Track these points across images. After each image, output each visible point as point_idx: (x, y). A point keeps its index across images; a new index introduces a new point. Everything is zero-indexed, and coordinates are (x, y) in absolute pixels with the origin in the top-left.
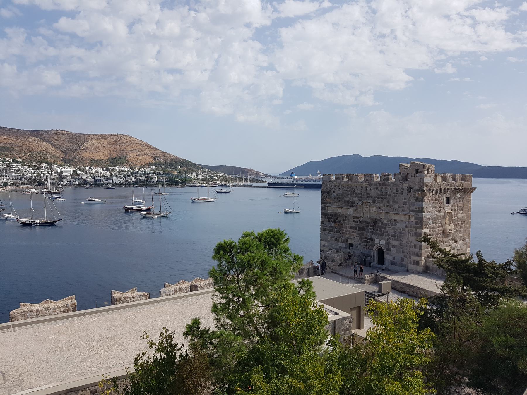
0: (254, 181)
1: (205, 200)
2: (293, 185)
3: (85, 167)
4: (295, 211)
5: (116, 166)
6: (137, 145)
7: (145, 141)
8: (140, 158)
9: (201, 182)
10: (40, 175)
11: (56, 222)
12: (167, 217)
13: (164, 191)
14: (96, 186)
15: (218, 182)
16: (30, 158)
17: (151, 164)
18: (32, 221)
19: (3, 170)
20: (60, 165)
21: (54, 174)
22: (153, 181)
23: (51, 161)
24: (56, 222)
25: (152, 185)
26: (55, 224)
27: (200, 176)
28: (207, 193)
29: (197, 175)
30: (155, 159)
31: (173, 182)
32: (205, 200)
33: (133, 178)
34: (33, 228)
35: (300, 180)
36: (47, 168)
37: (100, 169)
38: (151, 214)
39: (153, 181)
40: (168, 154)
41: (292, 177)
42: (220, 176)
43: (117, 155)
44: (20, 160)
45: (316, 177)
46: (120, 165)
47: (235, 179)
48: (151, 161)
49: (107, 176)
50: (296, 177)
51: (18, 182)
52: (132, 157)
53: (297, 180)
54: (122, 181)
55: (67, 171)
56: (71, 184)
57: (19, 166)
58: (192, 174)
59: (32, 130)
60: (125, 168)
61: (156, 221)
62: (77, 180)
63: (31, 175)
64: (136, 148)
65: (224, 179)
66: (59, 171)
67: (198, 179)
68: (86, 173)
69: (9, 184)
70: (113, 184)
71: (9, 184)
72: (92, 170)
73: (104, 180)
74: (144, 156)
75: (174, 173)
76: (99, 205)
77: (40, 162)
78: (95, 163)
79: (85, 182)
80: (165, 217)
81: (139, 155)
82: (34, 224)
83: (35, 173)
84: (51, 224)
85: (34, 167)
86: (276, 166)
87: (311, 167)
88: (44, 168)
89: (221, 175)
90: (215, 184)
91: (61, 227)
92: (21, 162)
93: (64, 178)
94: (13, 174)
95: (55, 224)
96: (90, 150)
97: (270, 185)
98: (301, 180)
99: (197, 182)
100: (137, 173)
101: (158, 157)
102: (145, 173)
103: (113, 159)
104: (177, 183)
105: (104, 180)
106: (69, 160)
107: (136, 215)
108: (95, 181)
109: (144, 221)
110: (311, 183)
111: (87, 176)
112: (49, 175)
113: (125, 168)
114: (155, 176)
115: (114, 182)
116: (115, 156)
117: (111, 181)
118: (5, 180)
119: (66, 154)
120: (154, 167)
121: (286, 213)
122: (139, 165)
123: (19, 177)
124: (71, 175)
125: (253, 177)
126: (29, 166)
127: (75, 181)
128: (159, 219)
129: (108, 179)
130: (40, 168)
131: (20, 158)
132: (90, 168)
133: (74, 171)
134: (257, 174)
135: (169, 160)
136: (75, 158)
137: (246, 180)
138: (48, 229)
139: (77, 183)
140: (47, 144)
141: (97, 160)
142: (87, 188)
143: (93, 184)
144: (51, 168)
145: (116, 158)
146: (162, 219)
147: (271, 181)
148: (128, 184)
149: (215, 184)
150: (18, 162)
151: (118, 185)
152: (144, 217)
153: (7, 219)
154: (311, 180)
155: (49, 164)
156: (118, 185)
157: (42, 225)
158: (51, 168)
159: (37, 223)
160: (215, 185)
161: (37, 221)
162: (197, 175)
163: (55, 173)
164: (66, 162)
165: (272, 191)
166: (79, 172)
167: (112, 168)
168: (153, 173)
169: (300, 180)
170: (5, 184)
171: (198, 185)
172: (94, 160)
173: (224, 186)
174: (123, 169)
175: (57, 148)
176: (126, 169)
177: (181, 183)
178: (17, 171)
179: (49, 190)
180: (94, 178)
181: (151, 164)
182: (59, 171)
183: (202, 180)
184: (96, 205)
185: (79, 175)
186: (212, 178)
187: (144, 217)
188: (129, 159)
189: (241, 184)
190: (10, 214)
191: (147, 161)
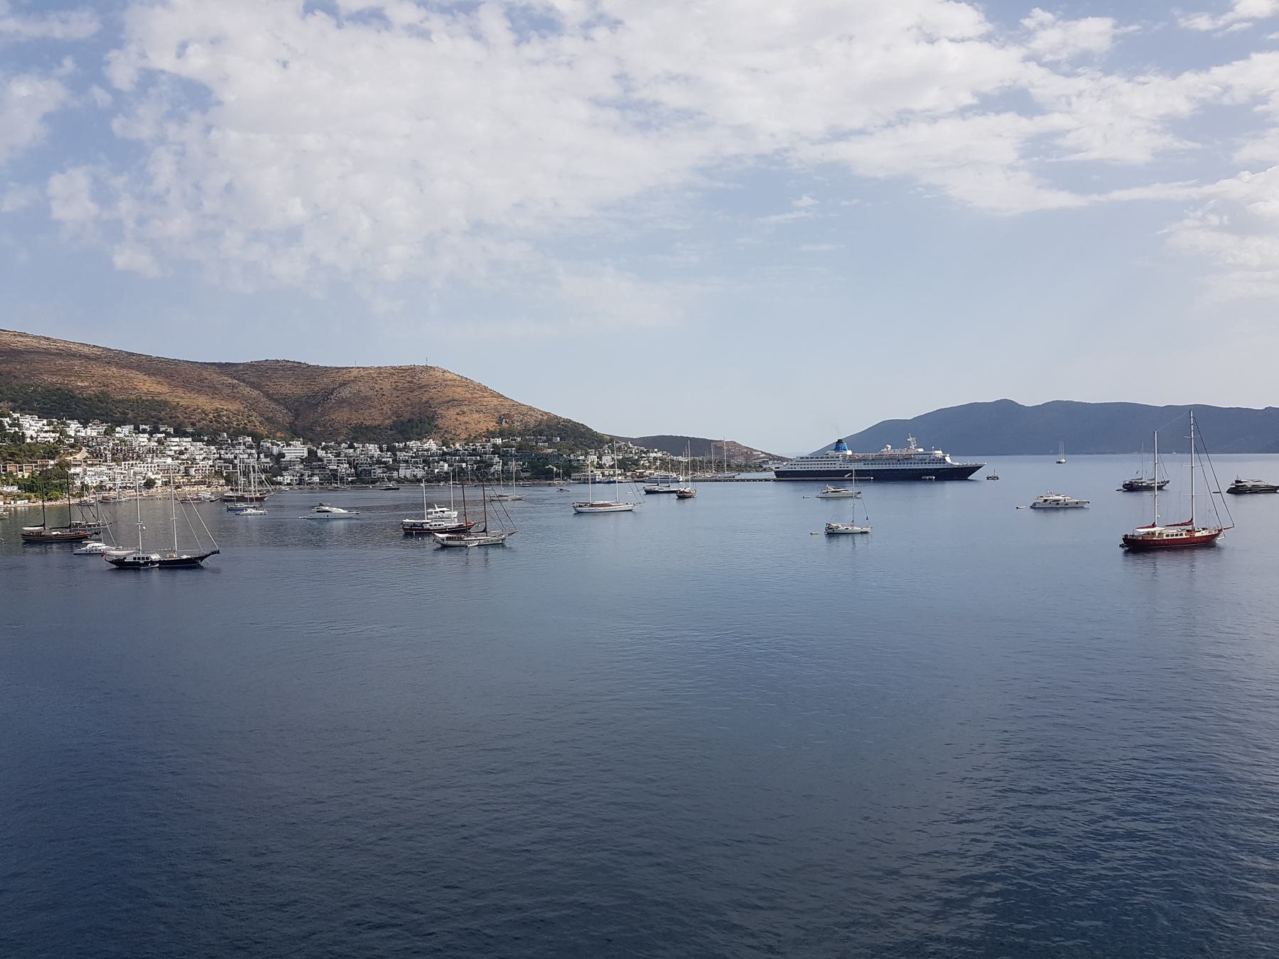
0: (740, 468)
1: (607, 508)
2: (843, 473)
3: (339, 444)
4: (857, 529)
5: (410, 440)
6: (459, 390)
7: (477, 381)
8: (466, 419)
9: (606, 473)
10: (231, 462)
11: (202, 558)
12: (503, 545)
13: (512, 492)
14: (358, 485)
15: (648, 472)
16: (215, 425)
17: (492, 434)
18: (141, 555)
19: (149, 451)
20: (281, 439)
21: (264, 460)
22: (492, 470)
23: (262, 430)
24: (202, 558)
25: (489, 480)
26: (202, 563)
27: (607, 460)
28: (625, 494)
29: (600, 458)
30: (500, 421)
31: (539, 471)
32: (607, 508)
33: (446, 465)
34: (142, 574)
35: (859, 460)
36: (251, 447)
37: (373, 449)
38: (461, 539)
39: (492, 470)
40: (531, 408)
41: (840, 454)
42: (655, 459)
43: (413, 413)
44: (190, 430)
45: (904, 452)
46: (420, 438)
47: (694, 466)
48: (492, 426)
49: (385, 463)
50: (849, 452)
51: (179, 479)
52: (449, 417)
53: (852, 460)
54: (420, 473)
55: (297, 450)
56: (301, 482)
57: (186, 442)
58: (587, 454)
59: (223, 361)
60: (432, 445)
61: (475, 556)
62: (316, 471)
63: (211, 463)
64: (457, 397)
65: (664, 465)
66: (275, 450)
67: (600, 466)
68: (338, 455)
69: (159, 483)
70: (399, 481)
71: (159, 483)
72: (355, 449)
73: (379, 471)
74: (476, 416)
75: (547, 453)
76: (342, 522)
77: (235, 434)
78: (361, 433)
79: (334, 476)
80: (499, 545)
81: (464, 413)
82: (146, 564)
83: (220, 458)
84: (191, 564)
85: (220, 446)
86: (799, 440)
87: (890, 430)
88: (242, 447)
89: (660, 455)
90: (641, 475)
91: (216, 571)
92: (192, 435)
93: (286, 469)
94: (169, 461)
95: (202, 563)
96: (350, 404)
97: (782, 476)
98: (864, 460)
99: (598, 472)
100: (456, 452)
101: (507, 416)
102: (474, 453)
103: (403, 423)
104: (549, 476)
105: (378, 472)
106: (304, 428)
107: (429, 542)
108: (357, 475)
109: (443, 556)
110: (891, 467)
111: (339, 462)
112: (252, 461)
113: (432, 445)
114: (496, 459)
115: (402, 476)
116: (407, 416)
117: (395, 474)
118: (150, 474)
119: (297, 416)
120: (499, 441)
121: (832, 534)
122: (464, 436)
123: (182, 467)
124: (302, 461)
125: (740, 460)
126: (208, 443)
127: (312, 475)
128: (483, 550)
129: (389, 468)
130: (233, 446)
131: (193, 424)
132: (351, 446)
133: (310, 451)
134: (748, 453)
135: (532, 424)
136: (316, 422)
137: (719, 467)
138: (183, 576)
139: (316, 479)
140: (255, 393)
141: (367, 428)
142: (336, 489)
143: (352, 482)
144: (258, 446)
145: (410, 421)
146: (491, 551)
147: (784, 467)
148: (433, 479)
149: (641, 475)
150: (185, 434)
151: (411, 481)
152: (444, 547)
153: (90, 554)
154: (891, 458)
155: (257, 438)
156: (411, 481)
157: (169, 566)
158: (258, 446)
159: (153, 563)
160: (640, 479)
161: (155, 557)
162: (600, 458)
163: (266, 456)
164: (294, 433)
165: (786, 489)
166: (321, 453)
167: (402, 445)
168: (493, 453)
169: (859, 460)
170: (150, 484)
171: (599, 477)
172: (360, 427)
173: (665, 480)
174: (426, 446)
175: (276, 400)
176: (434, 447)
177: (558, 475)
178: (181, 453)
179: (240, 493)
180: (355, 468)
181: (492, 434)
182: (275, 450)
183: (612, 467)
184: (335, 523)
185: (321, 460)
186: (636, 463)
187: (444, 547)
188: (439, 422)
189: (708, 476)
190: (99, 540)
191: (483, 427)
